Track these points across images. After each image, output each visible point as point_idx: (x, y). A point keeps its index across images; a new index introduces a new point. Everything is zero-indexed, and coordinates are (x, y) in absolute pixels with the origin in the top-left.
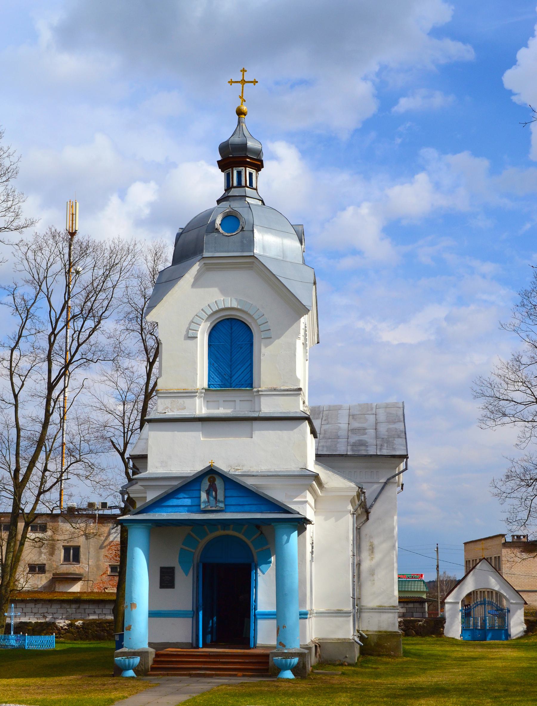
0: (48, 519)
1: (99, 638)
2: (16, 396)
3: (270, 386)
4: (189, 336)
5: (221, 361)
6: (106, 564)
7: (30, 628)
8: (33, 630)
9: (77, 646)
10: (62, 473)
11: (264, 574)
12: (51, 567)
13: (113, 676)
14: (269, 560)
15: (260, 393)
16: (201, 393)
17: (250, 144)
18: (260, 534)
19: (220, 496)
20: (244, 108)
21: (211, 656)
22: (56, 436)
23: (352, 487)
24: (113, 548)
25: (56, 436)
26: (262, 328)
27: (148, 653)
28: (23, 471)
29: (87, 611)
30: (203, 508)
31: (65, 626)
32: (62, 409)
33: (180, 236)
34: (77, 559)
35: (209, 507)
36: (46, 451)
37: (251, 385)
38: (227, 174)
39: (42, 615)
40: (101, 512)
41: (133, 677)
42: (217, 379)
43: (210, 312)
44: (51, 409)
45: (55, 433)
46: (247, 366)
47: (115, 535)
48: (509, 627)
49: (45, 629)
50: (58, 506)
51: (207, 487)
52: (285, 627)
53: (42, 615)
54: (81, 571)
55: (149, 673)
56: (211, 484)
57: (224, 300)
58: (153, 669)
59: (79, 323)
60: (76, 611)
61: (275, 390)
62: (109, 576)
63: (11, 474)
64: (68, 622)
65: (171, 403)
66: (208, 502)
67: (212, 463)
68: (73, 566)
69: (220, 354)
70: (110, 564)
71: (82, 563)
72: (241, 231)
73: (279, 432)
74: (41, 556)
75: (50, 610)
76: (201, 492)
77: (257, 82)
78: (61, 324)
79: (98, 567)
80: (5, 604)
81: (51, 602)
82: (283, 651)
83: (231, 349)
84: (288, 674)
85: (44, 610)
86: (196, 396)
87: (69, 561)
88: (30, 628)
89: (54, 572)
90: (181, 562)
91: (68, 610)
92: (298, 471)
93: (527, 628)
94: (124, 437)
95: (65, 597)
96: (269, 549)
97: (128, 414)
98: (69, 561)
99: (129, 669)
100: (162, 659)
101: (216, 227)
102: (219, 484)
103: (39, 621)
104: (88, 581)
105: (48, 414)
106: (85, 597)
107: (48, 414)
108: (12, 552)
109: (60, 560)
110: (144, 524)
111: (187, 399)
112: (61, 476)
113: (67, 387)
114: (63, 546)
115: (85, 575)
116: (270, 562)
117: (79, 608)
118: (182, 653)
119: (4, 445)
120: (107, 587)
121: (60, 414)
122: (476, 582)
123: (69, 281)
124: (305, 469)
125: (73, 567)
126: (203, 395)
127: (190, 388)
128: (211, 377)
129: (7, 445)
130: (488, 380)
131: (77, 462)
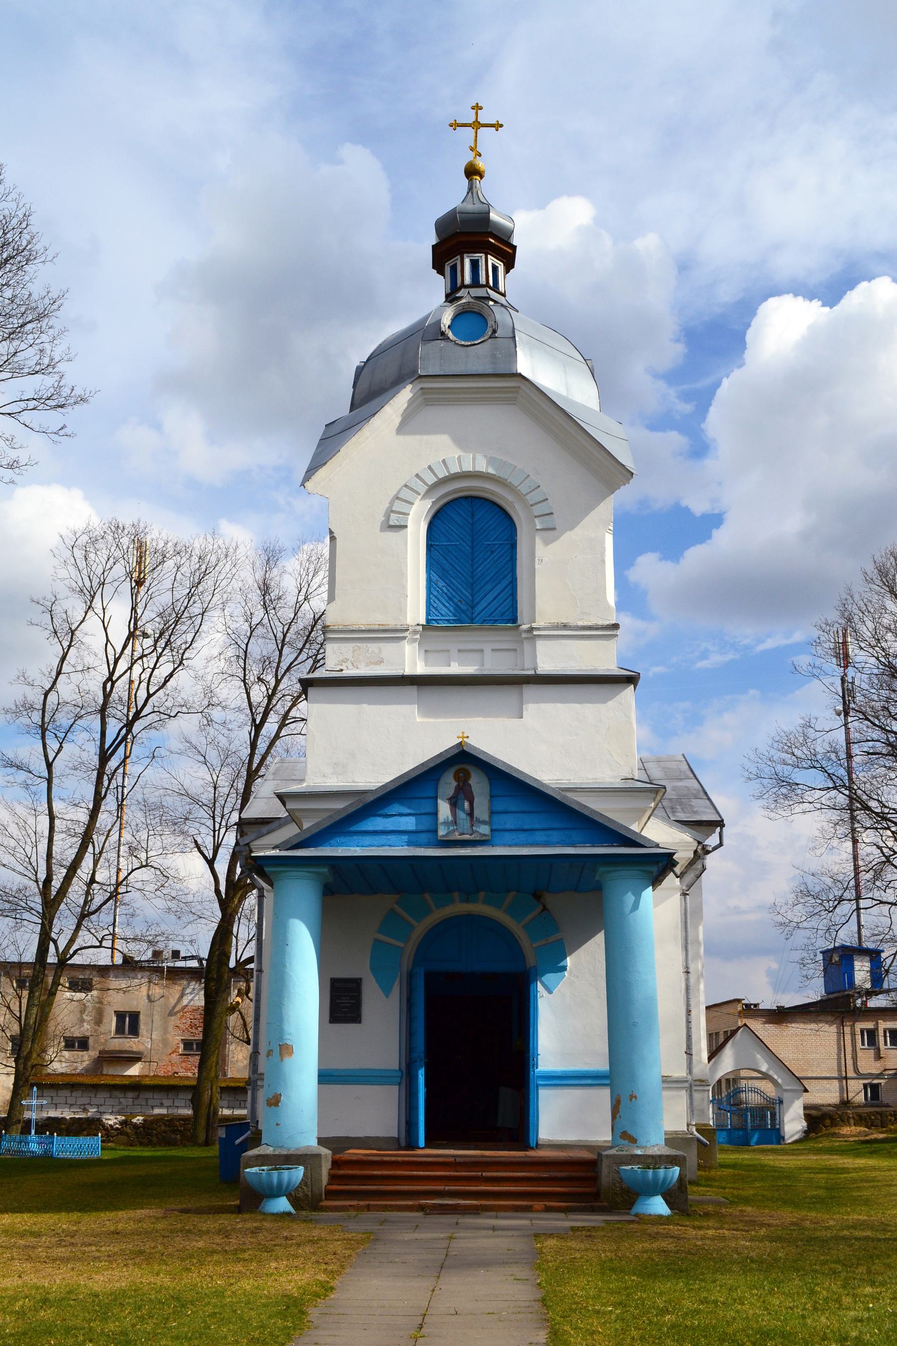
0: (95, 973)
1: (169, 1143)
2: (49, 765)
3: (555, 620)
4: (391, 523)
5: (452, 577)
6: (177, 1038)
7: (63, 1126)
8: (67, 1129)
9: (136, 1154)
10: (118, 884)
11: (550, 992)
12: (96, 1041)
13: (239, 1210)
14: (561, 964)
15: (535, 633)
16: (415, 632)
17: (493, 216)
18: (543, 911)
19: (481, 809)
20: (481, 164)
21: (460, 1164)
22: (110, 831)
23: (686, 842)
24: (188, 1015)
25: (110, 831)
26: (537, 510)
27: (321, 1159)
28: (56, 884)
29: (150, 1102)
30: (443, 836)
31: (116, 1124)
32: (120, 789)
33: (360, 373)
34: (134, 1031)
35: (457, 833)
36: (94, 854)
37: (514, 620)
38: (451, 267)
39: (82, 1107)
40: (171, 964)
41: (289, 1214)
42: (444, 611)
43: (431, 480)
44: (104, 790)
45: (108, 828)
46: (504, 586)
47: (190, 997)
48: (782, 1126)
49: (86, 1128)
50: (110, 934)
51: (451, 792)
52: (636, 1097)
53: (82, 1107)
54: (141, 1048)
55: (321, 1204)
56: (461, 785)
57: (459, 458)
58: (331, 1194)
59: (150, 661)
60: (133, 1102)
61: (565, 627)
62: (181, 1055)
63: (38, 885)
64: (121, 1118)
65: (354, 651)
66: (455, 822)
67: (463, 737)
68: (129, 1040)
69: (451, 564)
70: (183, 1038)
71: (143, 1036)
72: (490, 338)
73: (577, 706)
74: (83, 1026)
75: (95, 1101)
76: (439, 801)
77: (501, 126)
78: (122, 665)
79: (165, 1042)
80: (22, 1086)
81: (96, 1087)
82: (632, 1153)
83: (472, 554)
84: (658, 1206)
85: (85, 1100)
86: (404, 638)
87: (123, 1033)
88: (63, 1126)
89: (101, 1048)
90: (374, 969)
91: (121, 1100)
92: (619, 783)
93: (808, 1126)
94: (214, 836)
95: (118, 1081)
96: (561, 940)
97: (221, 801)
98: (123, 1033)
99: (278, 1196)
100: (350, 1172)
101: (443, 329)
102: (478, 783)
103: (77, 1116)
104: (150, 1062)
105: (98, 797)
106: (147, 1082)
107: (98, 799)
108: (36, 1005)
109: (111, 1032)
110: (312, 870)
111: (385, 644)
112: (116, 889)
113: (128, 757)
114: (115, 1012)
115: (145, 1054)
116: (564, 968)
117: (138, 1097)
118: (393, 1159)
119: (28, 840)
120: (178, 1071)
121: (117, 798)
122: (737, 1059)
123: (136, 602)
124: (633, 779)
125: (129, 1042)
126: (418, 636)
127: (392, 623)
128: (433, 606)
129: (34, 841)
130: (767, 754)
131: (142, 866)
